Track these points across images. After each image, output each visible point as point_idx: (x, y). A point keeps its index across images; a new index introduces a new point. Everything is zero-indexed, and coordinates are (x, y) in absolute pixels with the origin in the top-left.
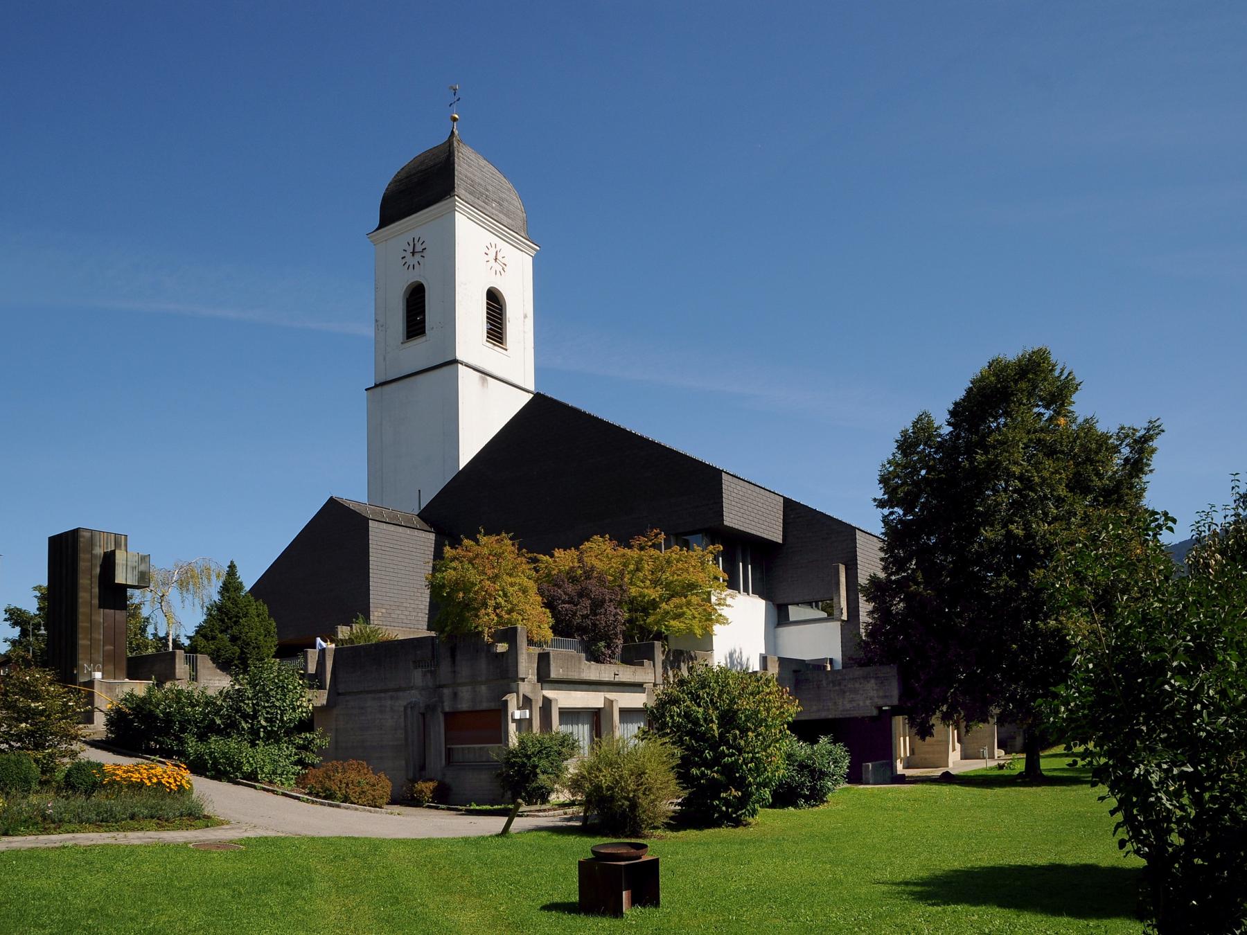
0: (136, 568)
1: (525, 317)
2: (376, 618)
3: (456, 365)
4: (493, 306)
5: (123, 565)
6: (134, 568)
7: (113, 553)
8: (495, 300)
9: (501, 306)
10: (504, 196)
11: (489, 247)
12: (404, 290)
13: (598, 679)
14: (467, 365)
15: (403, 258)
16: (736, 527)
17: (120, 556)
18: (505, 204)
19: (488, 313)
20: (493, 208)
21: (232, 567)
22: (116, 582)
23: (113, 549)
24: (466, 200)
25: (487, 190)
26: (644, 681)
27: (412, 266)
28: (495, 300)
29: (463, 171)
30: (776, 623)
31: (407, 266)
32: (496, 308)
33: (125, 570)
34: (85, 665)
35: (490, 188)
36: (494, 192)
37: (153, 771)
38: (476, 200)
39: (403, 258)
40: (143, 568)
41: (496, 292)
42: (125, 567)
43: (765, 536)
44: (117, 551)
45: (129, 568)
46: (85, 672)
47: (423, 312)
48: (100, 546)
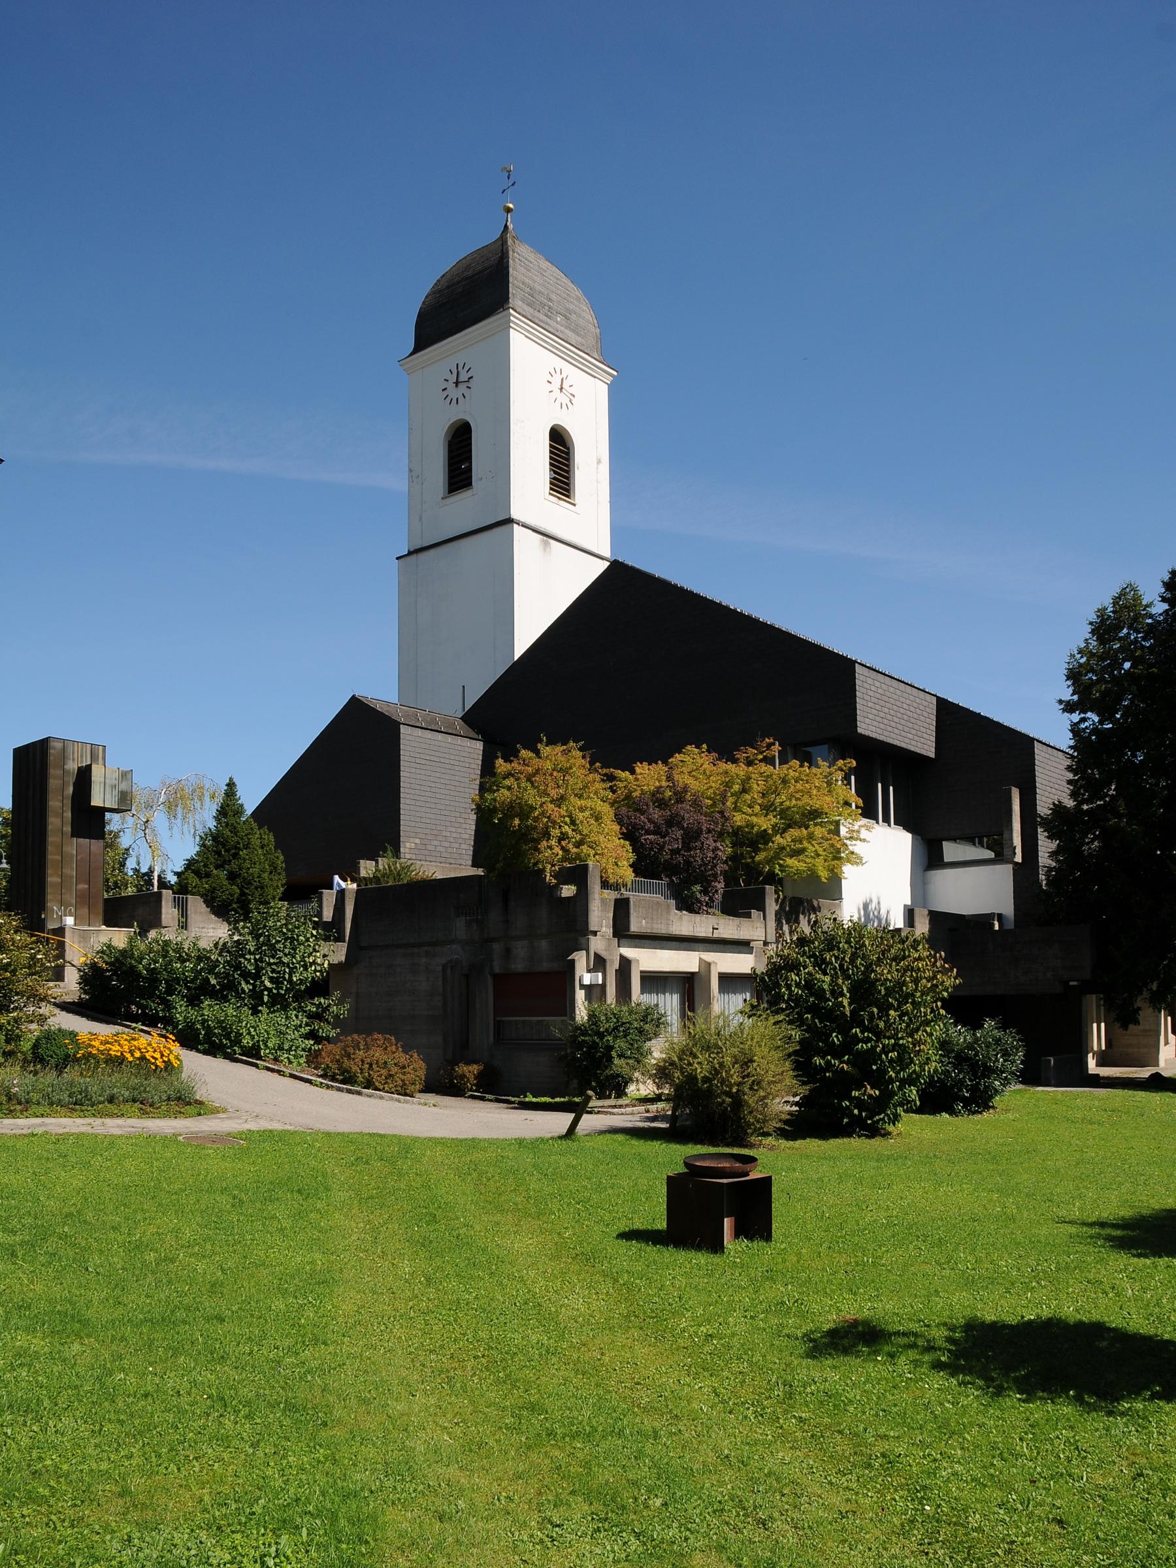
1: (599, 462)
2: (407, 850)
6: (113, 787)
8: (559, 441)
10: (572, 307)
11: (553, 373)
18: (573, 317)
23: (89, 763)
25: (550, 300)
28: (559, 441)
29: (520, 277)
34: (55, 908)
35: (553, 297)
37: (135, 1043)
42: (102, 785)
44: (94, 767)
48: (73, 760)
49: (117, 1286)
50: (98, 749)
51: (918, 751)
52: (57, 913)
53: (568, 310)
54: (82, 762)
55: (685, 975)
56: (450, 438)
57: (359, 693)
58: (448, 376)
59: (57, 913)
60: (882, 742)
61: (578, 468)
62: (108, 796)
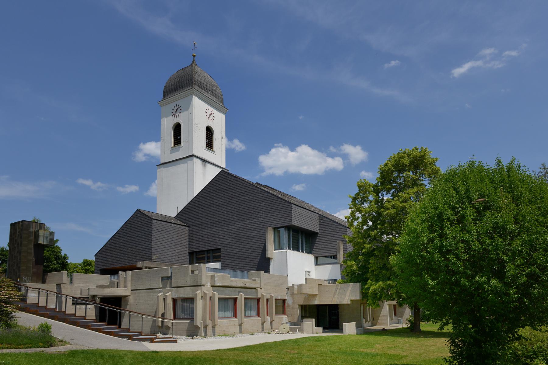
0: (48, 237)
1: (222, 138)
2: (154, 259)
3: (193, 157)
4: (209, 134)
5: (42, 236)
6: (47, 237)
7: (38, 231)
8: (209, 132)
9: (212, 134)
10: (214, 88)
11: (207, 109)
12: (173, 125)
13: (235, 285)
14: (198, 157)
15: (172, 113)
16: (298, 225)
17: (41, 232)
18: (214, 92)
19: (206, 136)
20: (209, 93)
21: (58, 240)
22: (39, 243)
23: (38, 229)
24: (198, 90)
25: (207, 86)
26: (257, 287)
27: (213, 119)
28: (209, 132)
29: (197, 78)
30: (316, 264)
31: (211, 120)
32: (210, 134)
33: (43, 238)
34: (23, 277)
35: (208, 85)
36: (210, 87)
37: (533, 218)
38: (202, 90)
39: (172, 113)
40: (51, 237)
41: (209, 127)
42: (43, 237)
43: (310, 229)
44: (40, 231)
45: (45, 237)
46: (23, 280)
47: (180, 135)
48: (33, 228)
49: (519, 209)
50: (42, 225)
51: (312, 230)
52: (24, 279)
53: (212, 89)
54: (36, 229)
55: (220, 306)
56: (174, 128)
57: (140, 208)
58: (174, 108)
59: (24, 279)
60: (298, 227)
61: (215, 140)
62: (45, 240)
